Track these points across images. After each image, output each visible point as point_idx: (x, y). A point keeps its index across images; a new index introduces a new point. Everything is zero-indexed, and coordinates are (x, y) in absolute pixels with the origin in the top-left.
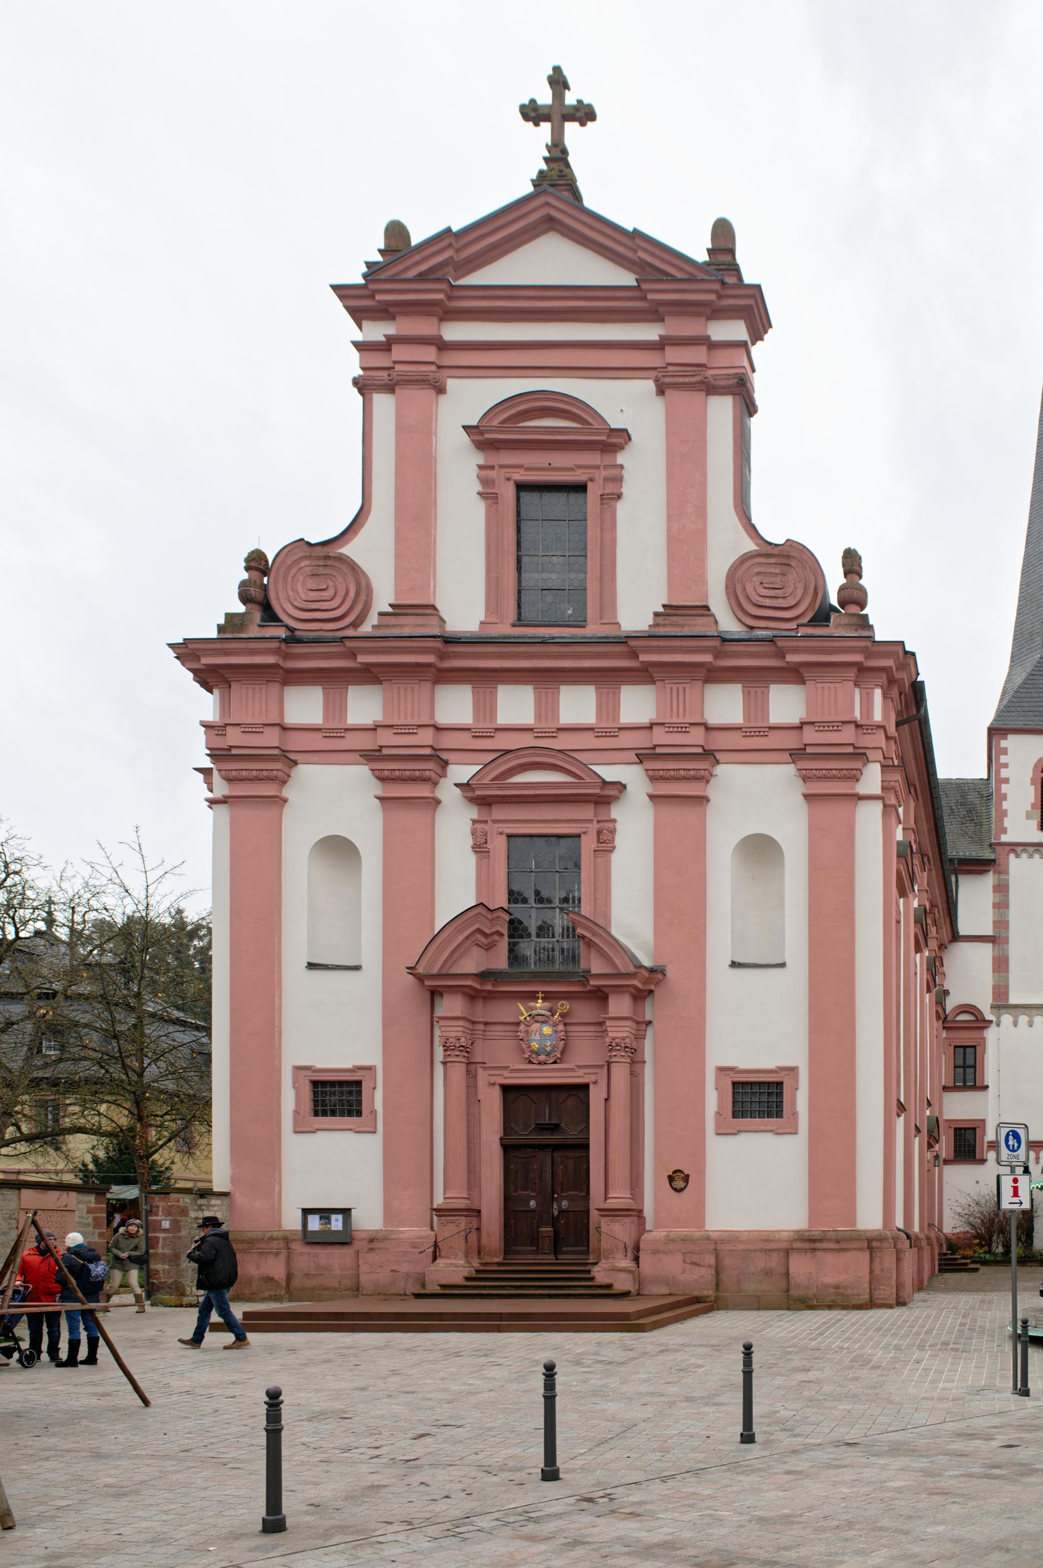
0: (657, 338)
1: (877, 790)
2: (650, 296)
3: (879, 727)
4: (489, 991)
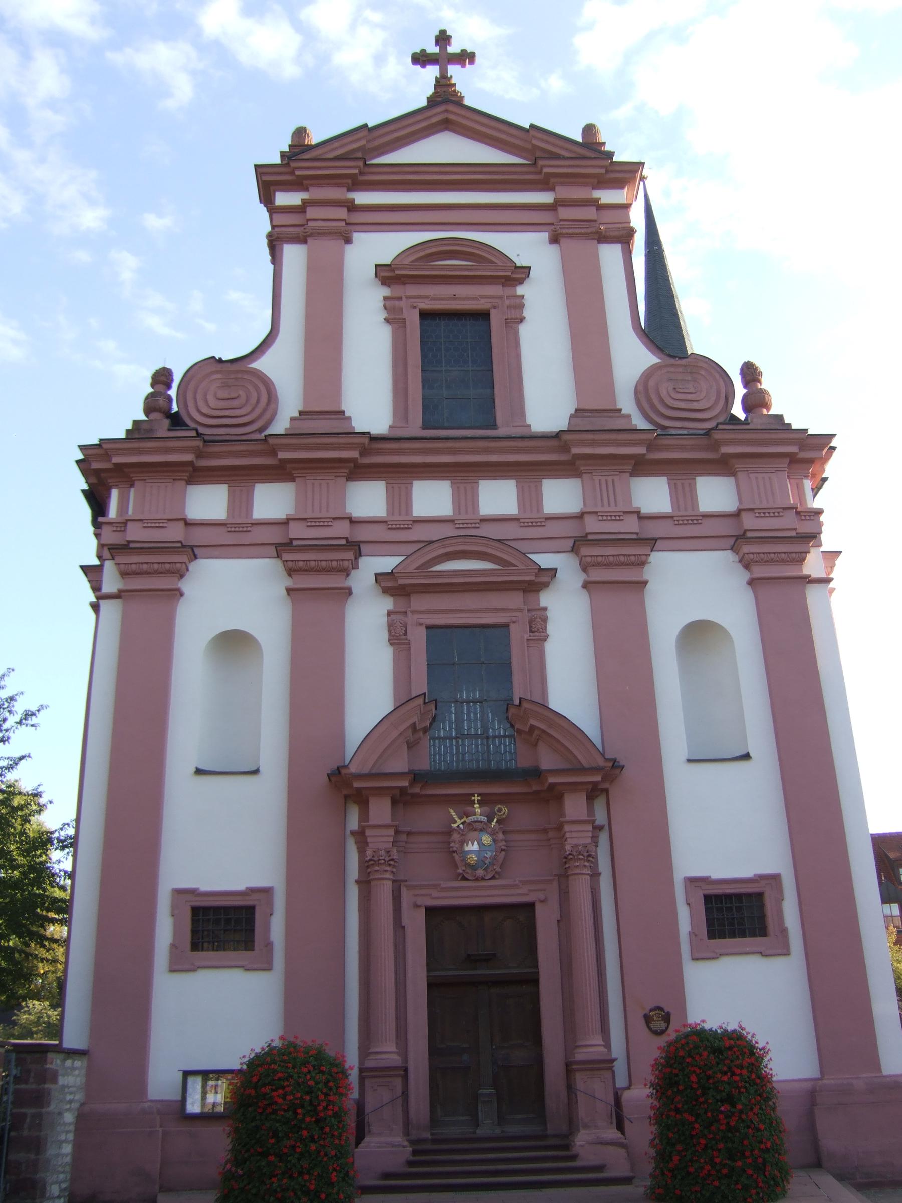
0: (299, 203)
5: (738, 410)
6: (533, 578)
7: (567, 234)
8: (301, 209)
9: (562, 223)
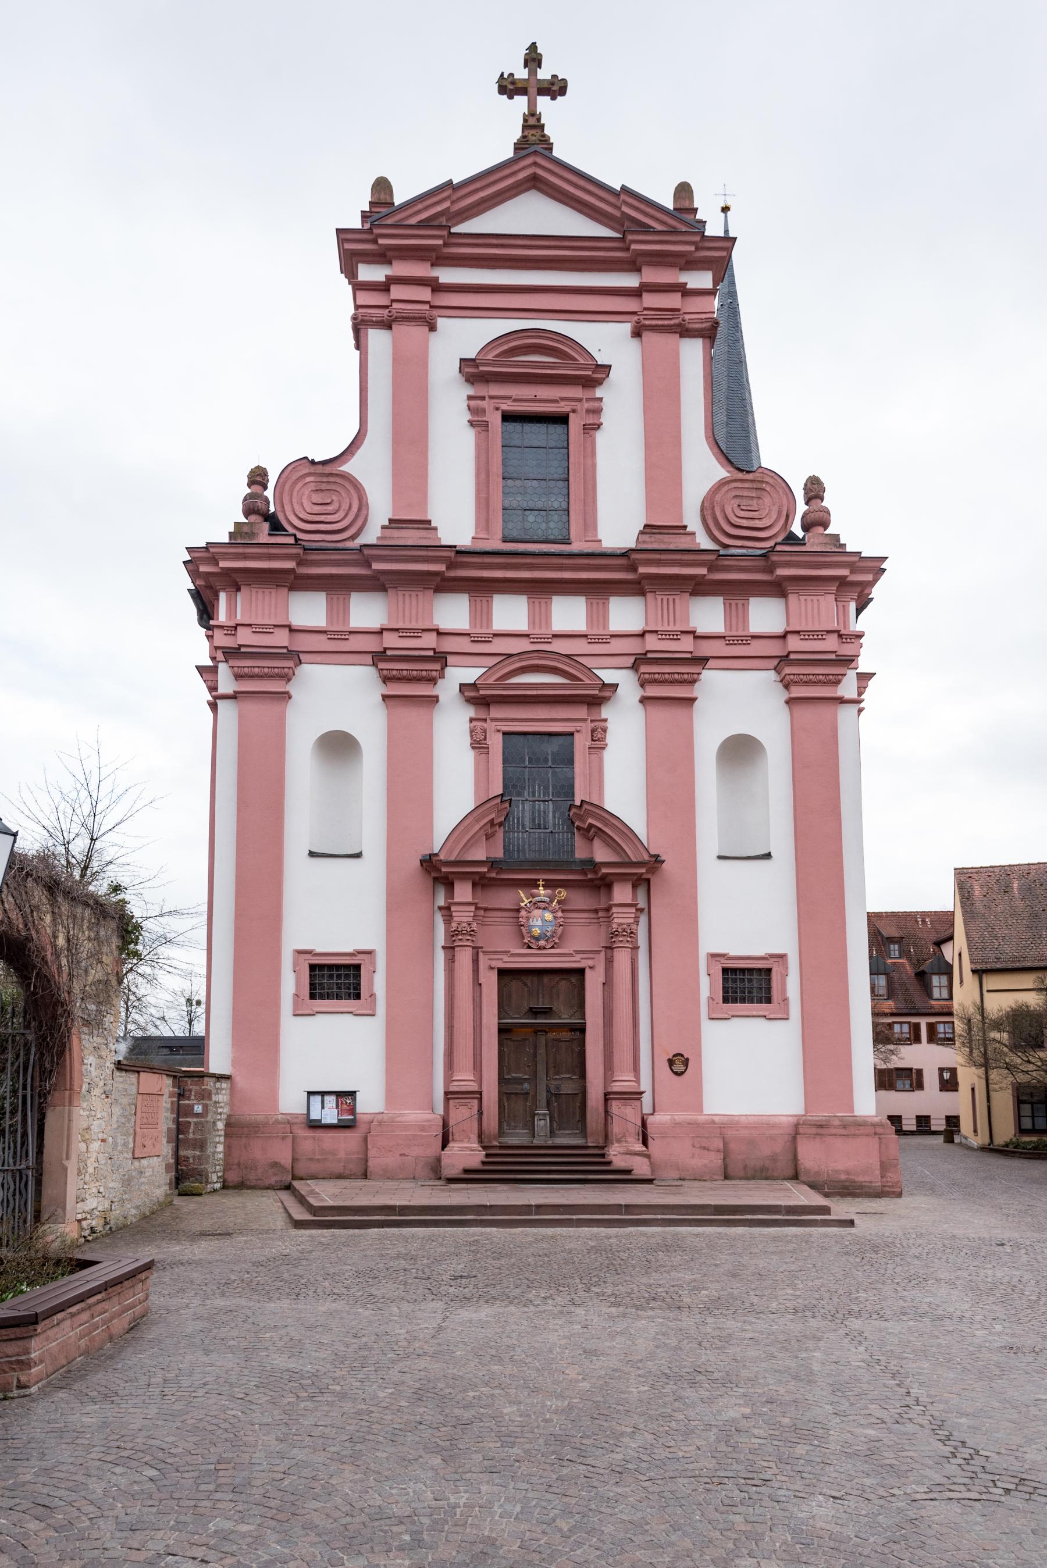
0: (384, 279)
4: (493, 879)
5: (797, 529)
6: (597, 692)
7: (650, 326)
8: (384, 287)
9: (645, 312)
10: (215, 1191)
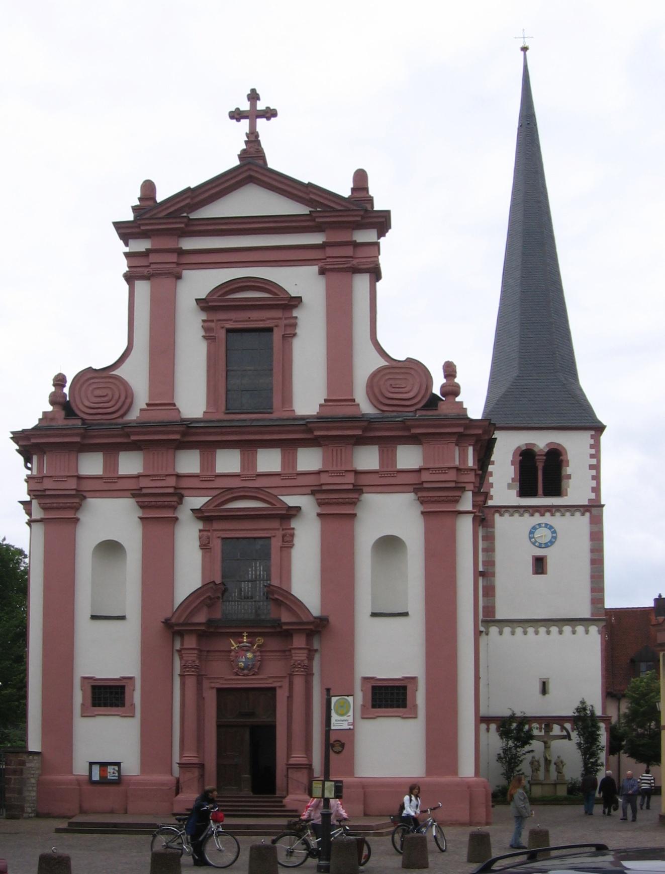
1: (470, 508)
2: (317, 220)
3: (472, 470)
10: (29, 817)
